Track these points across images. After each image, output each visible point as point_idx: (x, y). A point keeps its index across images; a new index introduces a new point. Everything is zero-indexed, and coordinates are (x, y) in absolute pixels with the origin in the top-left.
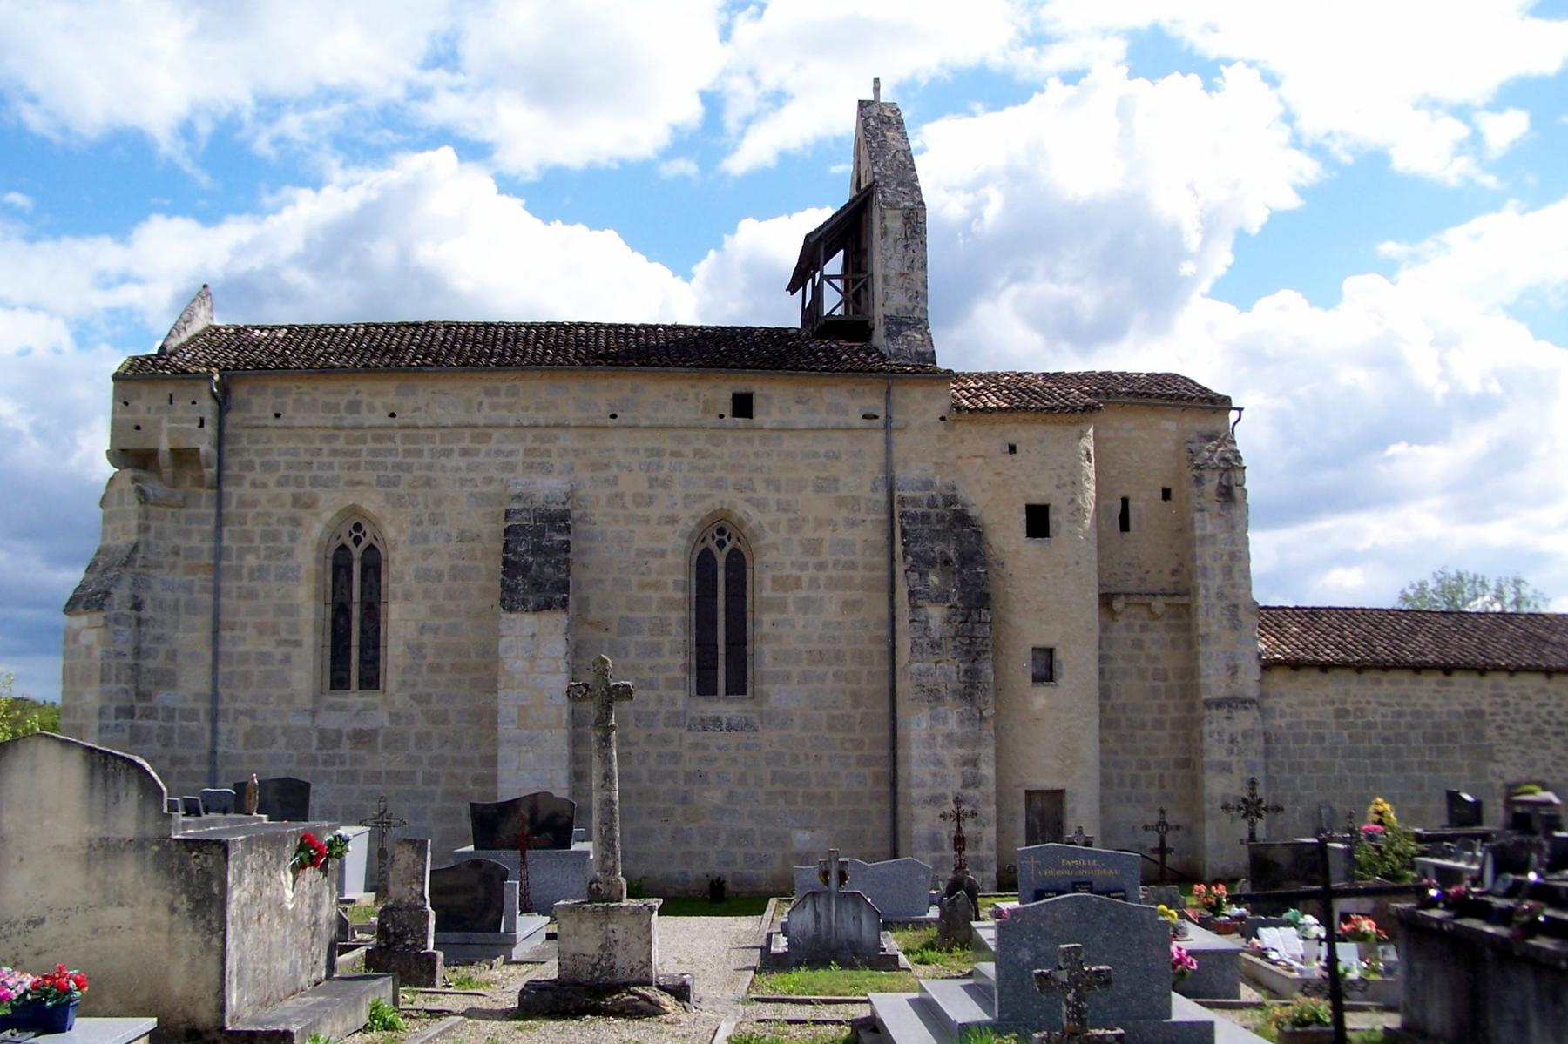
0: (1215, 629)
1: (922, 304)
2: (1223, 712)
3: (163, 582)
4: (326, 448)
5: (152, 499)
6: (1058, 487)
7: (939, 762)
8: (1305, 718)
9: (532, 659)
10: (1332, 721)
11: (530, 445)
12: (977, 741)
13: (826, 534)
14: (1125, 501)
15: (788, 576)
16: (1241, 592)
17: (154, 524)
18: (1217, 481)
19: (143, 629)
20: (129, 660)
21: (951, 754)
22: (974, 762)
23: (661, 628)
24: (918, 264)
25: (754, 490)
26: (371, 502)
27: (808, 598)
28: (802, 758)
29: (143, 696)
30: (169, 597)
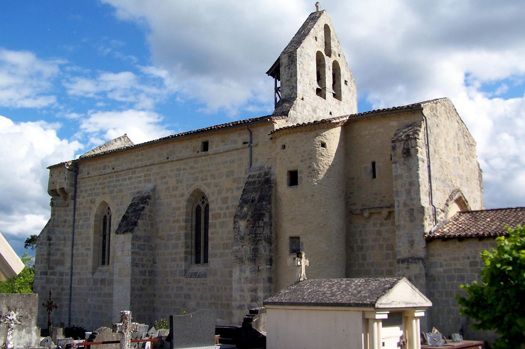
0: (402, 222)
1: (295, 91)
2: (405, 265)
3: (59, 231)
4: (98, 182)
5: (55, 205)
6: (302, 161)
7: (242, 290)
8: (453, 267)
9: (123, 251)
10: (468, 268)
11: (146, 173)
12: (255, 281)
13: (229, 194)
14: (374, 164)
15: (217, 213)
16: (415, 202)
17: (57, 213)
18: (402, 147)
19: (51, 247)
20: (46, 257)
21: (247, 286)
22: (255, 290)
23: (178, 238)
24: (293, 74)
25: (207, 180)
26: (108, 200)
27: (223, 222)
28: (220, 289)
29: (52, 268)
30: (62, 236)
